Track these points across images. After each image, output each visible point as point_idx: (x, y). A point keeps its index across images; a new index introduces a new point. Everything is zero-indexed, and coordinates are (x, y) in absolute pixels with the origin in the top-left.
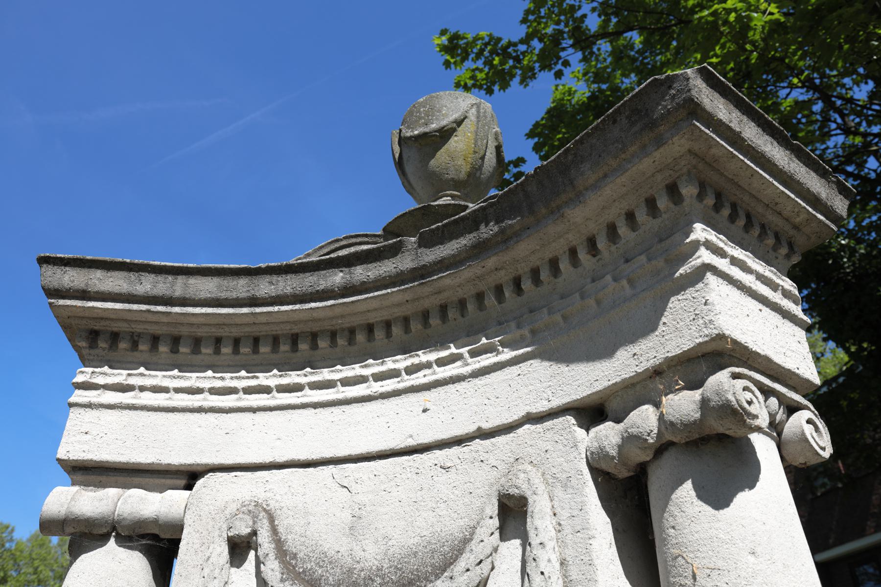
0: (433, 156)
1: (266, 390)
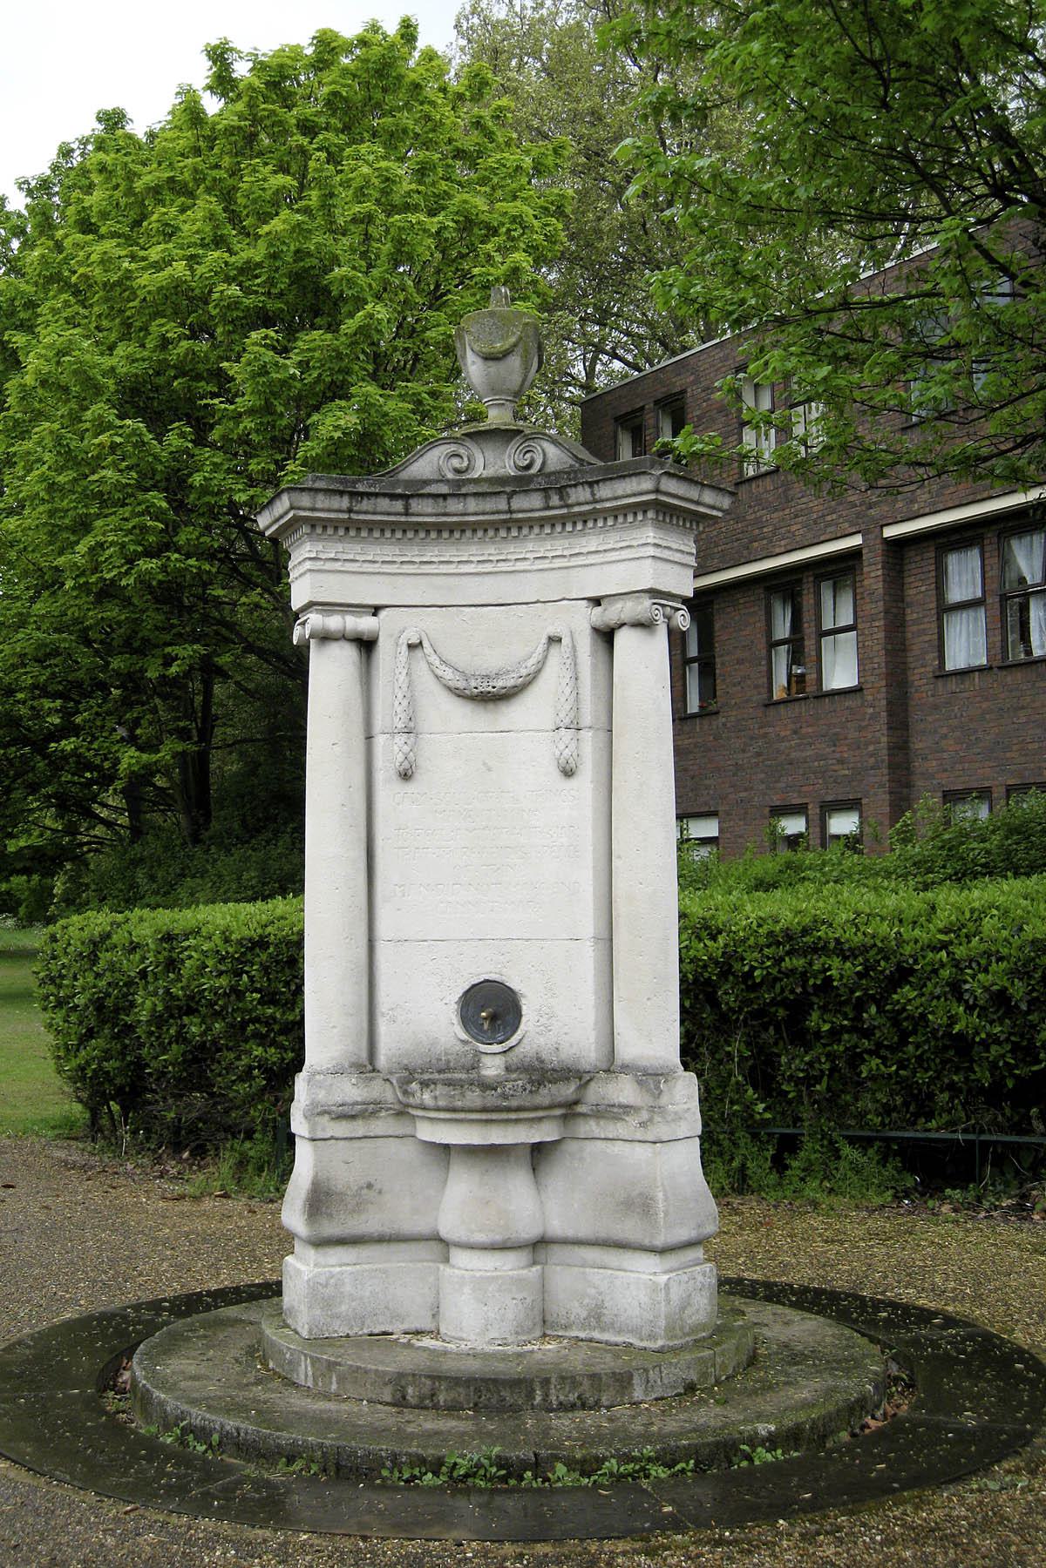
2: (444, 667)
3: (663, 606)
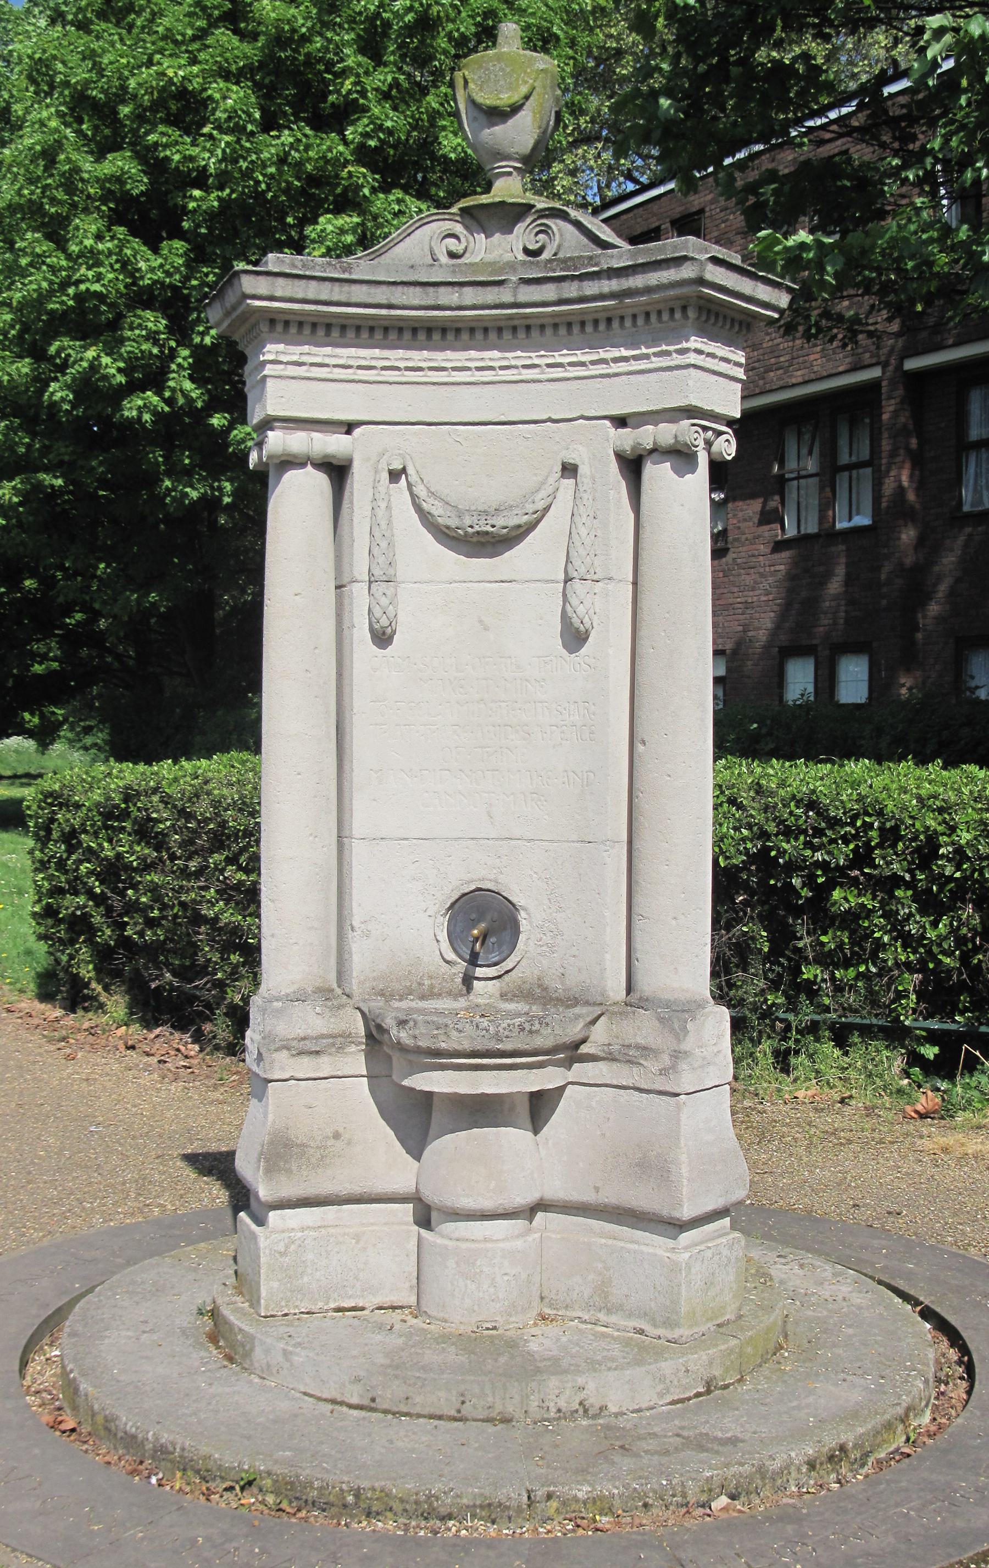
2: (431, 501)
3: (705, 429)
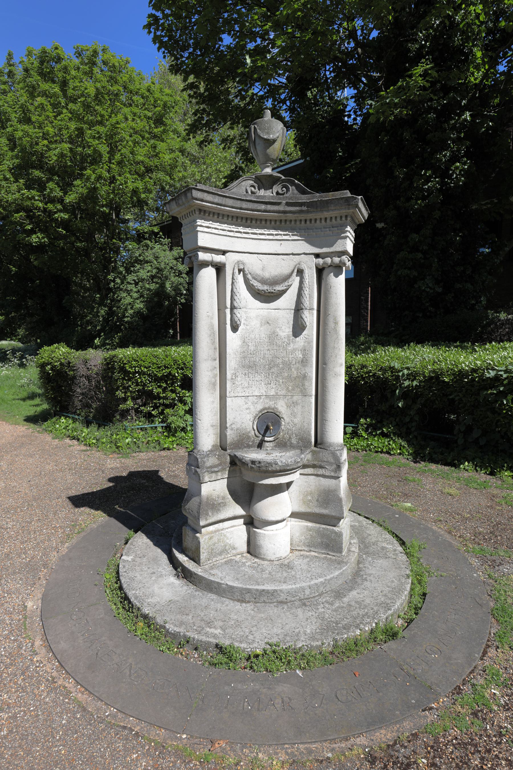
0: (269, 148)
1: (240, 232)
2: (253, 280)
